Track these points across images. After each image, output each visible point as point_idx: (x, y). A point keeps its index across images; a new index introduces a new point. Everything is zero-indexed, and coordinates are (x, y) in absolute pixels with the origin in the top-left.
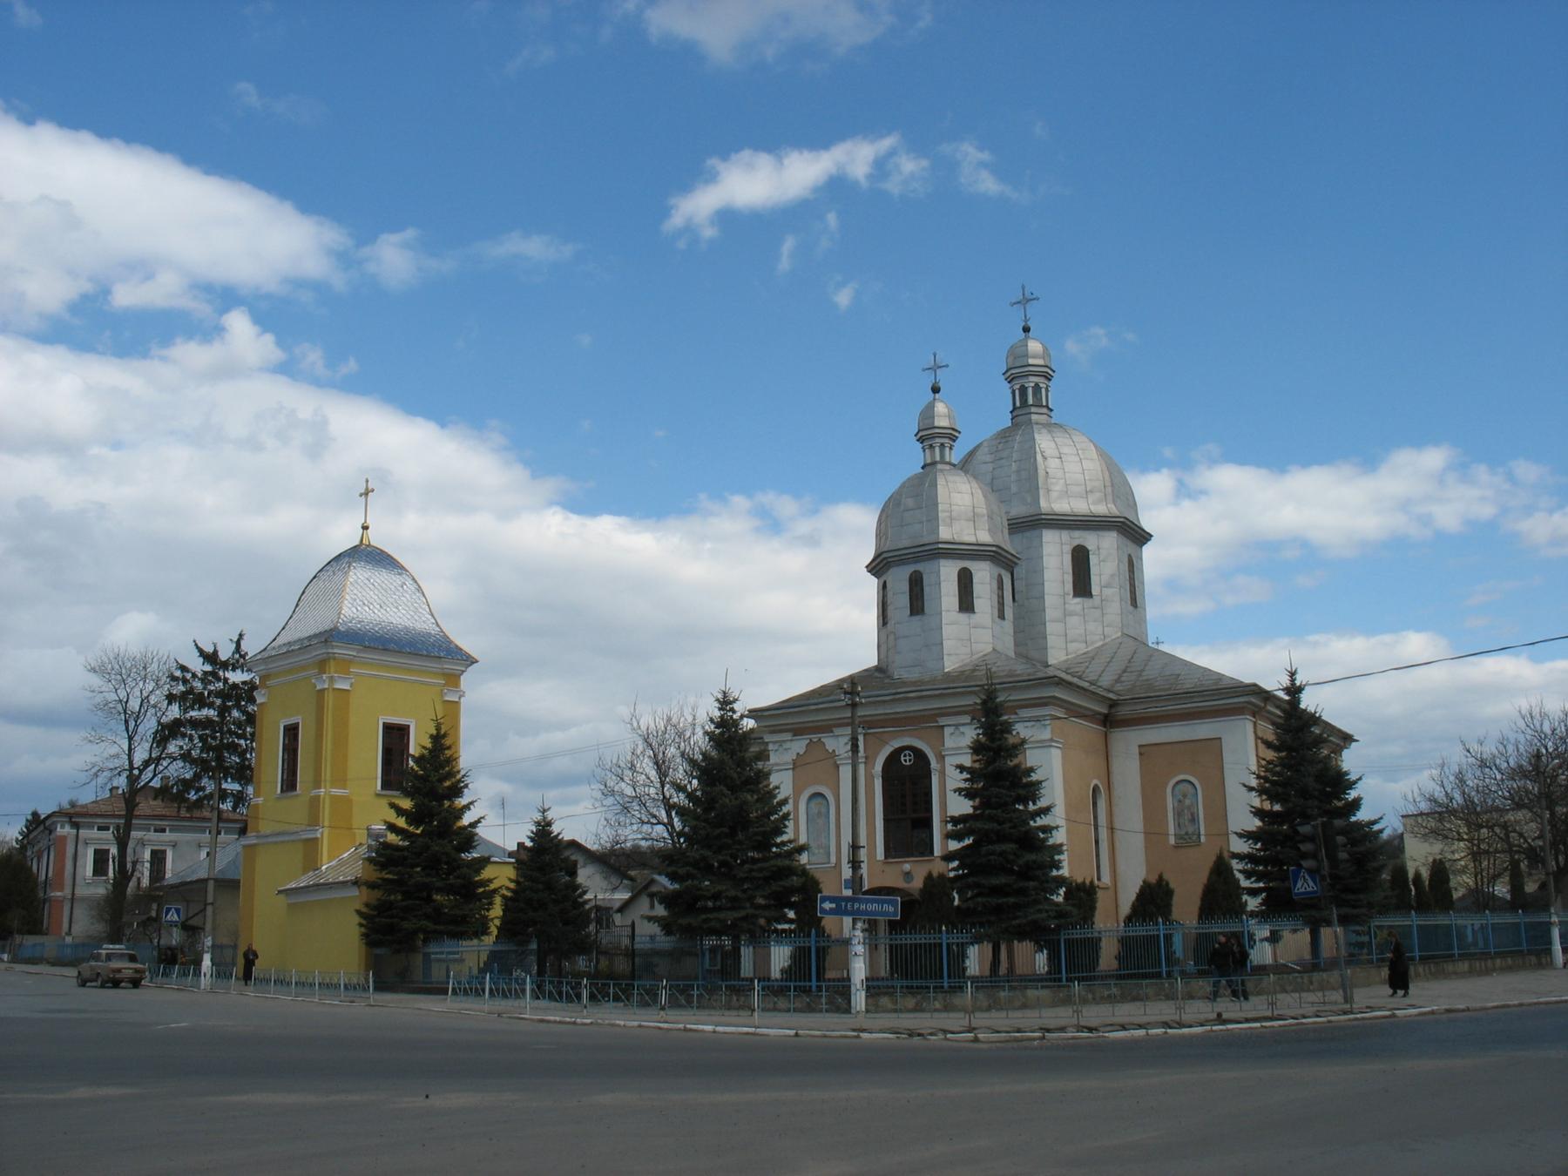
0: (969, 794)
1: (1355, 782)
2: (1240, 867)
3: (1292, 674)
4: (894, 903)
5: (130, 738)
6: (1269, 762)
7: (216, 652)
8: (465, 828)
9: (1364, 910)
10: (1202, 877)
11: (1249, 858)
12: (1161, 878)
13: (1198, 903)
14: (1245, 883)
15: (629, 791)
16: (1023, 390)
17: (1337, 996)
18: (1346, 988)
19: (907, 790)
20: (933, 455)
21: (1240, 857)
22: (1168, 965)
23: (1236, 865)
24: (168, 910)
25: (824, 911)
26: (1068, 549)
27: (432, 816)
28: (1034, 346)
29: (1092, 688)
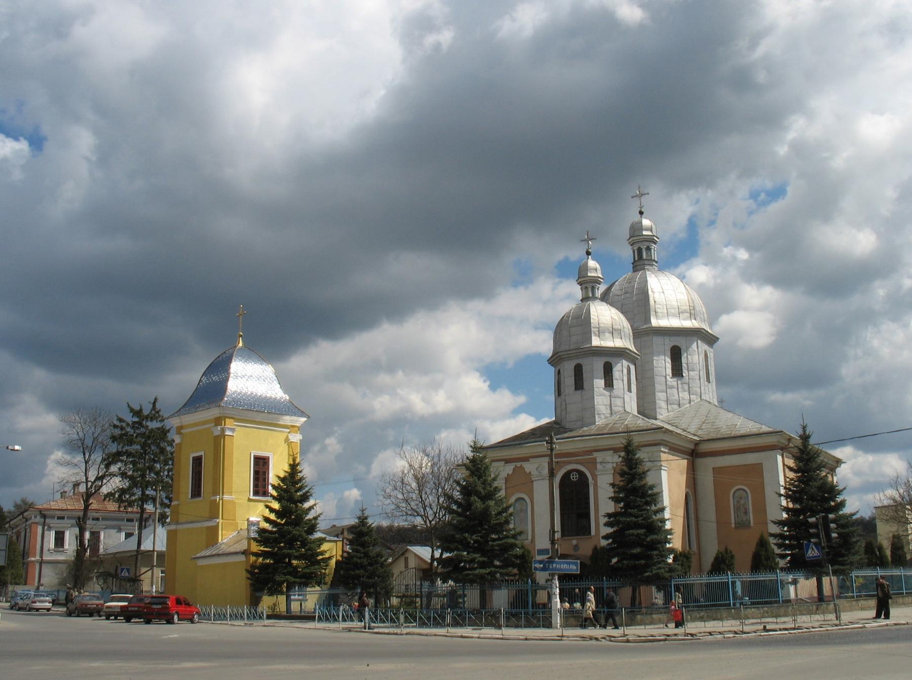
0: (616, 500)
1: (842, 491)
2: (775, 541)
3: (804, 428)
4: (576, 564)
5: (86, 462)
6: (791, 480)
7: (141, 410)
8: (310, 520)
9: (848, 567)
10: (752, 547)
11: (781, 536)
12: (726, 549)
13: (750, 563)
14: (777, 551)
15: (400, 496)
16: (640, 250)
17: (832, 616)
18: (837, 612)
19: (574, 497)
20: (587, 293)
21: (774, 536)
22: (734, 600)
23: (772, 541)
24: (122, 570)
25: (536, 569)
26: (668, 348)
27: (291, 513)
28: (646, 222)
29: (683, 433)
